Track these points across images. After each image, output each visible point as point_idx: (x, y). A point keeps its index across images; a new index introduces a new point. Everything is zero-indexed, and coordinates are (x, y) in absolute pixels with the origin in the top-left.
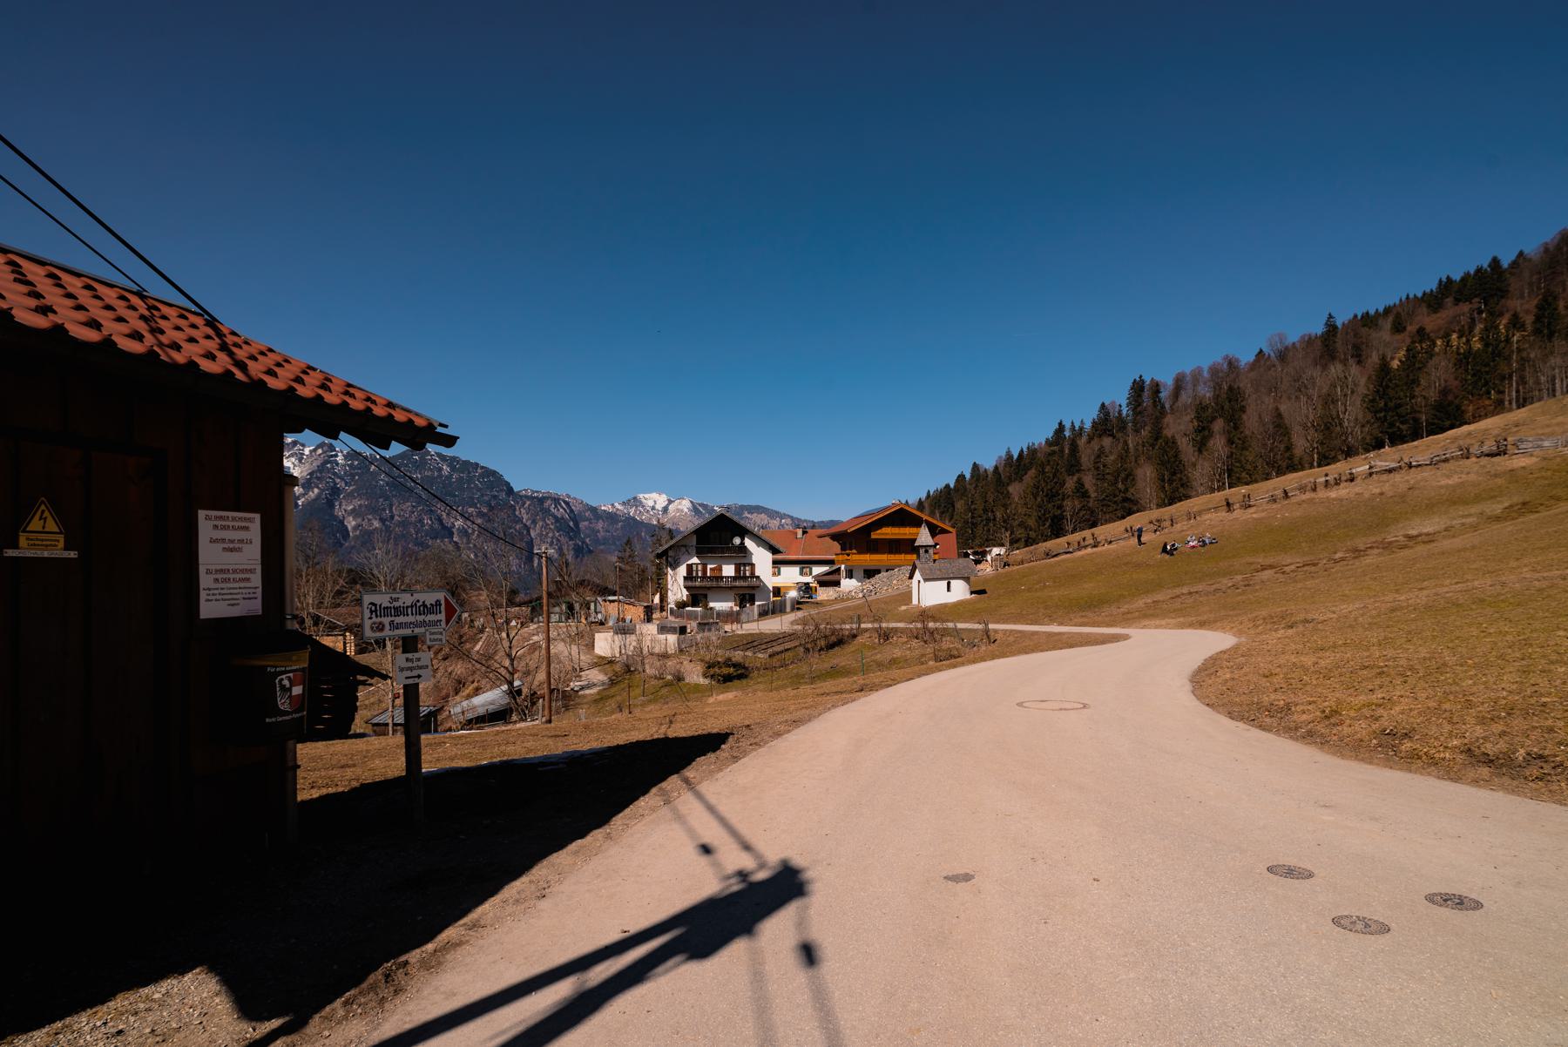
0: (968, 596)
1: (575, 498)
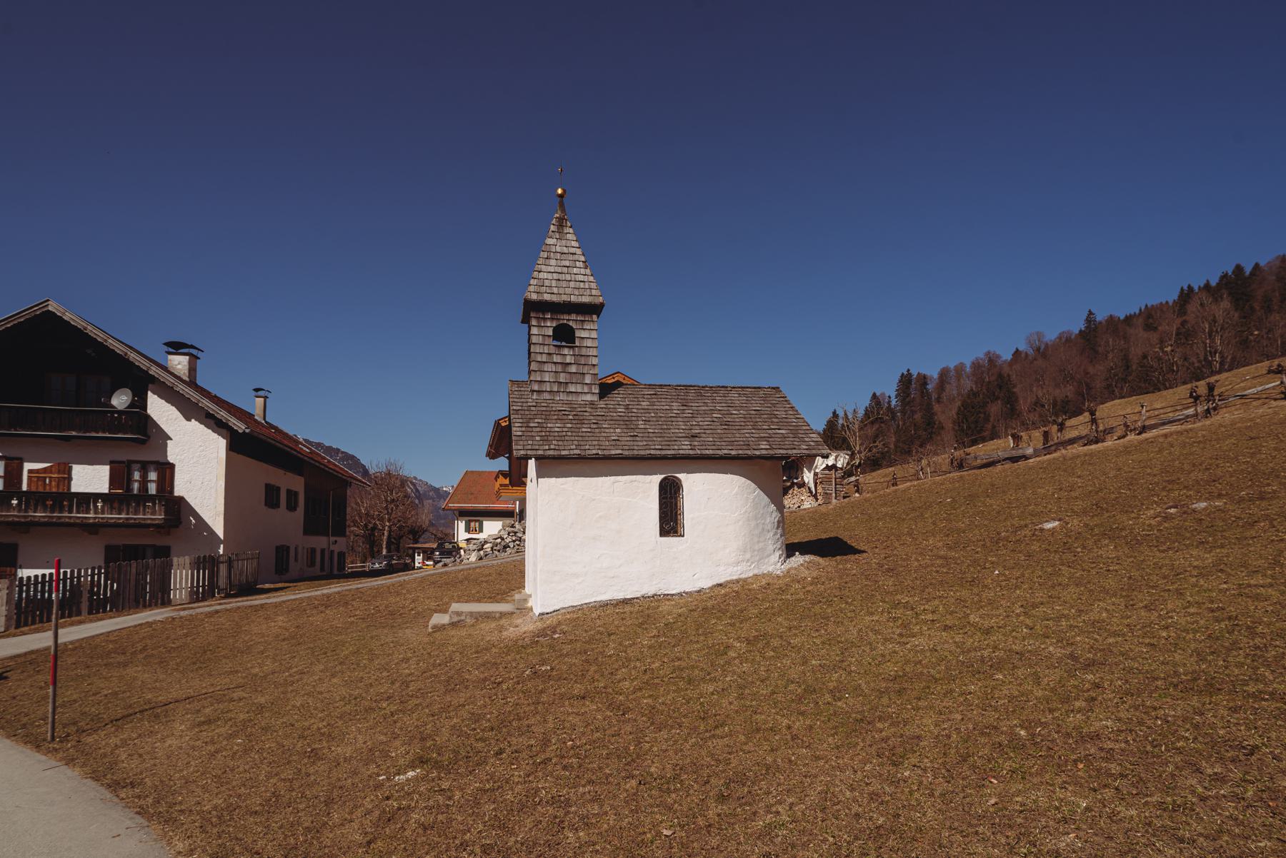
0: (774, 564)
1: (420, 480)
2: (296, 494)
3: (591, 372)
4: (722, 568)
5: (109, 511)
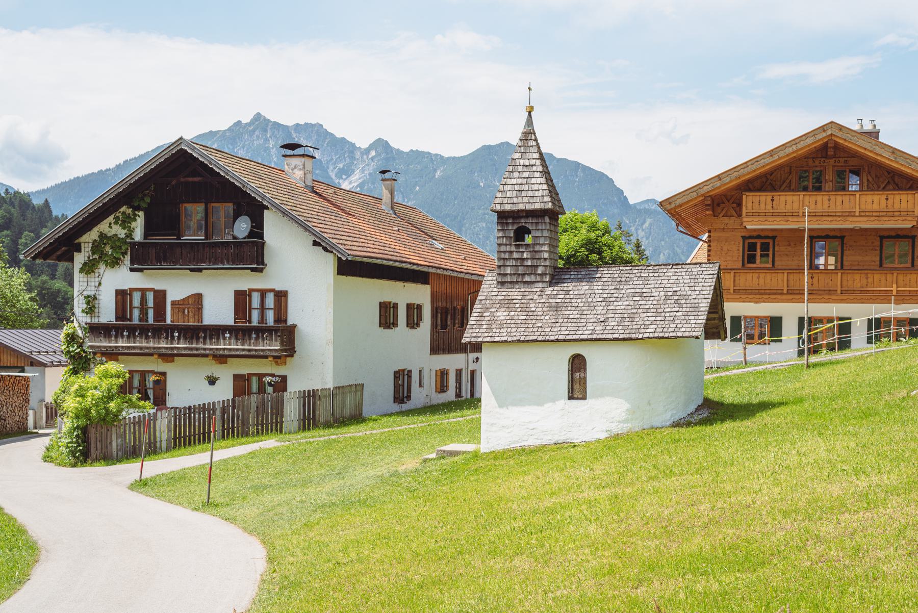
2: (419, 307)
3: (543, 264)
4: (615, 424)
5: (235, 342)
